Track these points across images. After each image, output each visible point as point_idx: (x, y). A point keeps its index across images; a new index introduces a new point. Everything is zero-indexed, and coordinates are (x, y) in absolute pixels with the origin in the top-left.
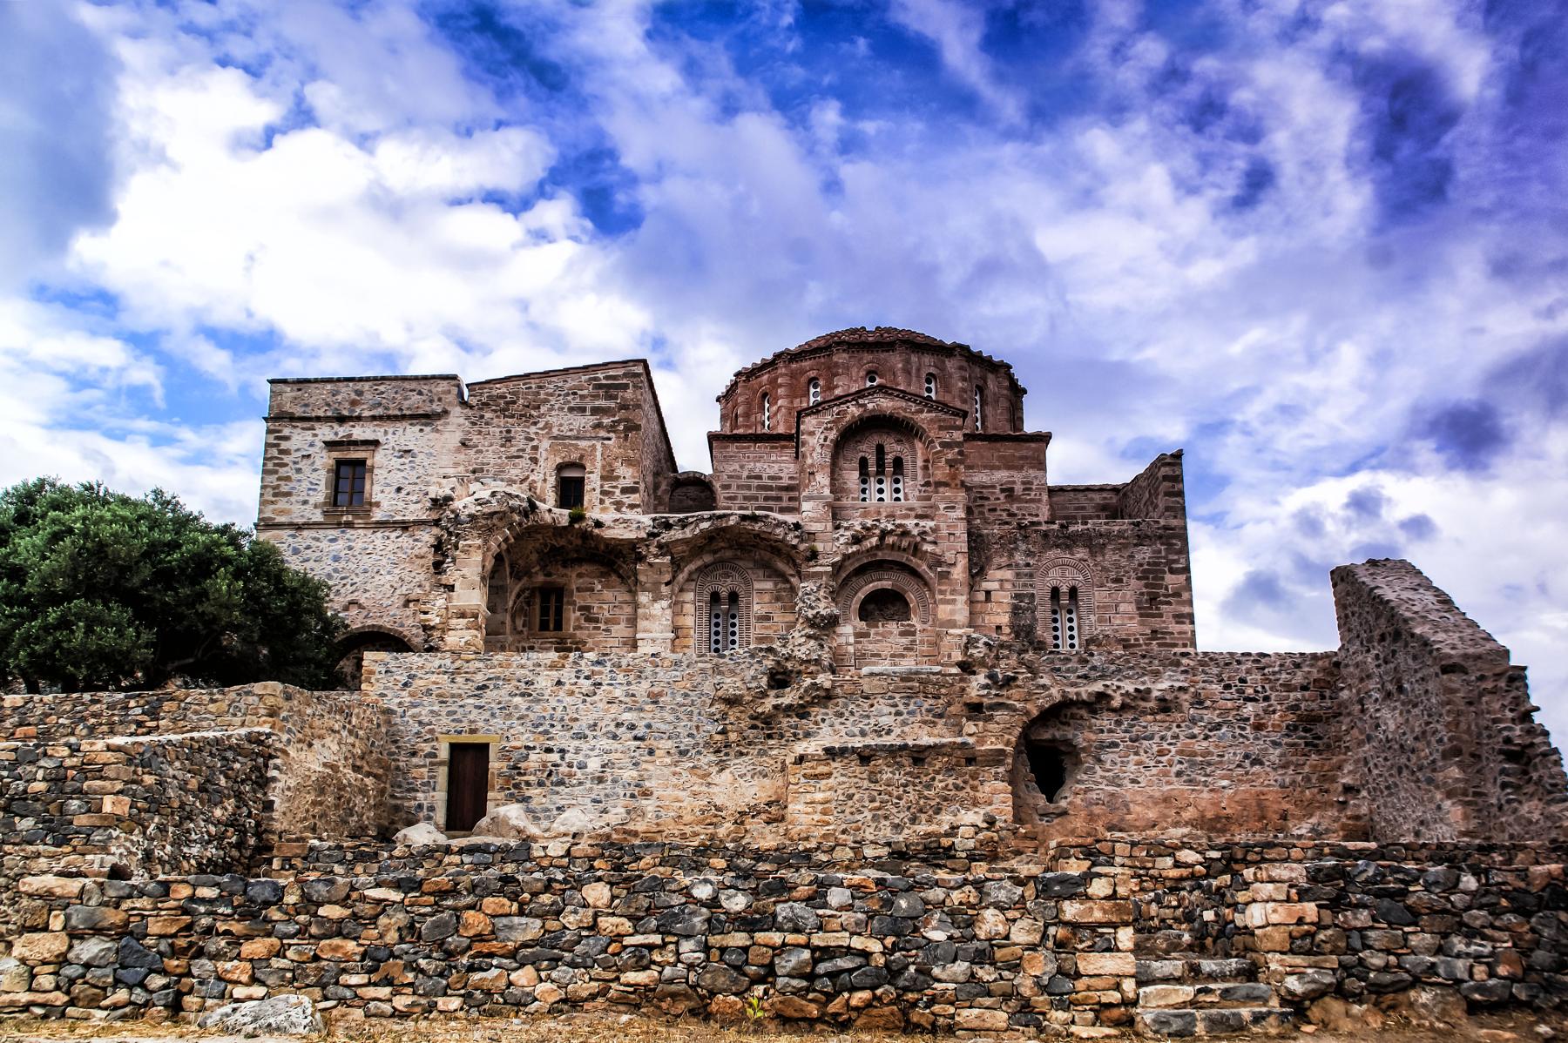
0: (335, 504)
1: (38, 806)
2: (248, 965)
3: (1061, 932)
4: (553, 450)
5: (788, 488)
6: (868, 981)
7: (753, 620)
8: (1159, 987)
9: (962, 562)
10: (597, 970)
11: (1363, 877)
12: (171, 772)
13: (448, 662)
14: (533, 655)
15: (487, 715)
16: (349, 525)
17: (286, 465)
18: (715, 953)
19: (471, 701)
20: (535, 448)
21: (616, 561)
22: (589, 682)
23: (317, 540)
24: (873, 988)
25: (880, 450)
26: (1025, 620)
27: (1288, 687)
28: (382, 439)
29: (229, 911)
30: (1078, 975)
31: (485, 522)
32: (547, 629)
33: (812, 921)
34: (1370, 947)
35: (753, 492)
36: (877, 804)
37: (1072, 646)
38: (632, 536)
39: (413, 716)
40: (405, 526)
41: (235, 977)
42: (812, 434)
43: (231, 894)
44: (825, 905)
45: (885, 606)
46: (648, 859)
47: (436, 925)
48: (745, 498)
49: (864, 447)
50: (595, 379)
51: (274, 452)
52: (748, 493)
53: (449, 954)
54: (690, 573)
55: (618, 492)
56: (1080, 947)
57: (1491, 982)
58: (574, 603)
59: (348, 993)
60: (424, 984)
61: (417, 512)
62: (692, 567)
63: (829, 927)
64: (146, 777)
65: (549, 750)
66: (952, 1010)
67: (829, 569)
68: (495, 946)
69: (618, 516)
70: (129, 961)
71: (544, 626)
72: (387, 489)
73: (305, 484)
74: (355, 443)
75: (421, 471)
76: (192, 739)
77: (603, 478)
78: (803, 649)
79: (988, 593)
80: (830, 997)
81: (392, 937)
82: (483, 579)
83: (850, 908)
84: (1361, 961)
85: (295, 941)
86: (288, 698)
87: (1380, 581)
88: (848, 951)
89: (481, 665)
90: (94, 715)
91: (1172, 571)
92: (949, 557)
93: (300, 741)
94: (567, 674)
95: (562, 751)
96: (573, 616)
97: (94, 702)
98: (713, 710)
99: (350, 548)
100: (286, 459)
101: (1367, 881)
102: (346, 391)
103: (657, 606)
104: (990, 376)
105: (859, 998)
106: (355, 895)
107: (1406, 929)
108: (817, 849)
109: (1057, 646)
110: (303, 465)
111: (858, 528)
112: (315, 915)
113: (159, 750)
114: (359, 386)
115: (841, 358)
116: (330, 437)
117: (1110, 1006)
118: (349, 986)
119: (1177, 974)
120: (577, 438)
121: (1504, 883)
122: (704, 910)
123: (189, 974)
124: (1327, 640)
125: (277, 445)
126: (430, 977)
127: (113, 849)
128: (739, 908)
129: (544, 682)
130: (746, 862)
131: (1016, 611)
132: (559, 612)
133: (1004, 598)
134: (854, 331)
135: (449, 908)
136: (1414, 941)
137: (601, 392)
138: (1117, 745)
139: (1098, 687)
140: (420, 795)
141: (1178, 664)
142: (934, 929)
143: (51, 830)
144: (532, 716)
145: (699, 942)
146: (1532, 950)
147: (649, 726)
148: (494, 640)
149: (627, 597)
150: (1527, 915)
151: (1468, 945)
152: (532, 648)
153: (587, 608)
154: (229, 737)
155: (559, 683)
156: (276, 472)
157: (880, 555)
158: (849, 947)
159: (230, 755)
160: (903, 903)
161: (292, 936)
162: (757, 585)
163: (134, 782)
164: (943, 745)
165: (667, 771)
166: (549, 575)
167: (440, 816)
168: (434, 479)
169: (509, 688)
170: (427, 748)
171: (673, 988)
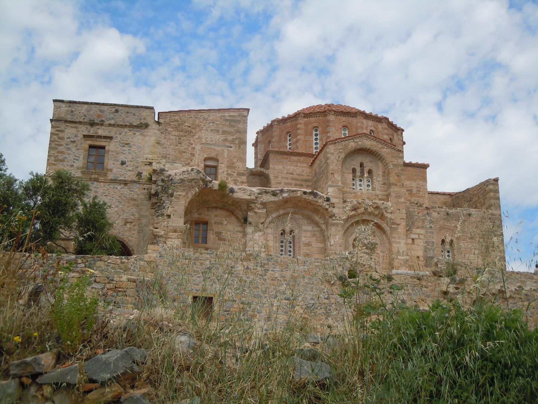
7: (302, 245)
9: (403, 223)
13: (192, 253)
17: (61, 145)
25: (362, 165)
26: (430, 254)
28: (114, 136)
35: (290, 181)
42: (332, 154)
49: (354, 163)
50: (224, 116)
51: (56, 137)
52: (287, 181)
55: (235, 175)
58: (213, 230)
61: (130, 176)
62: (274, 215)
72: (117, 163)
73: (72, 157)
74: (100, 137)
75: (134, 155)
77: (228, 167)
79: (413, 239)
89: (208, 256)
96: (211, 237)
100: (63, 142)
102: (95, 108)
103: (257, 234)
104: (395, 134)
111: (355, 202)
114: (102, 107)
115: (332, 118)
116: (86, 133)
120: (213, 144)
125: (58, 134)
131: (426, 250)
133: (420, 243)
137: (227, 123)
141: (532, 278)
149: (240, 229)
153: (220, 233)
156: (57, 149)
162: (304, 228)
166: (200, 214)
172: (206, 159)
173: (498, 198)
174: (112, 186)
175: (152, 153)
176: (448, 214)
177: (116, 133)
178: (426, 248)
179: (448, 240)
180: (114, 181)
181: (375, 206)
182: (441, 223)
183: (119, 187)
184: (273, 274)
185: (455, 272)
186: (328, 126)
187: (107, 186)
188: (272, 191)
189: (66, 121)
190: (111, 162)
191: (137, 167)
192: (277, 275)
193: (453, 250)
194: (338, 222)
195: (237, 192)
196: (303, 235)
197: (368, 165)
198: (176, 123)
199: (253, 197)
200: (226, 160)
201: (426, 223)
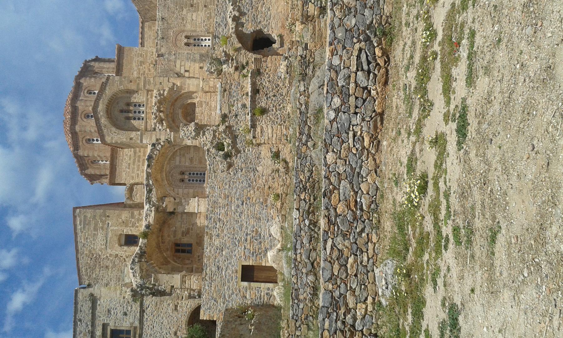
4: (112, 248)
9: (172, 80)
14: (205, 246)
15: (230, 266)
18: (357, 110)
19: (224, 273)
20: (111, 255)
21: (166, 217)
22: (218, 224)
24: (374, 47)
25: (122, 111)
26: (197, 57)
29: (335, 314)
31: (145, 275)
32: (191, 250)
36: (274, 109)
37: (209, 40)
38: (153, 213)
40: (142, 311)
42: (112, 138)
43: (328, 313)
46: (301, 177)
48: (138, 170)
53: (355, 218)
55: (133, 220)
58: (180, 239)
61: (136, 307)
63: (349, 65)
65: (246, 240)
66: (384, 17)
67: (172, 133)
71: (190, 252)
75: (117, 305)
81: (347, 243)
83: (341, 57)
85: (349, 285)
88: (358, 57)
92: (170, 85)
94: (214, 233)
95: (247, 235)
96: (185, 240)
105: (378, 52)
106: (329, 259)
108: (300, 110)
109: (209, 46)
111: (155, 121)
112: (338, 276)
115: (77, 128)
118: (368, 261)
123: (362, 331)
126: (365, 227)
128: (339, 101)
130: (304, 138)
132: (184, 245)
133: (188, 65)
137: (87, 227)
139: (230, 21)
147: (238, 199)
148: (196, 268)
149: (179, 216)
152: (199, 256)
155: (218, 236)
160: (340, 35)
161: (346, 285)
165: (257, 192)
167: (271, 285)
171: (372, 126)
174: (145, 323)
175: (115, 290)
176: (163, 38)
179: (186, 40)
181: (158, 104)
183: (146, 316)
184: (223, 215)
188: (148, 192)
190: (124, 324)
191: (128, 302)
192: (223, 211)
193: (193, 36)
195: (149, 222)
196: (183, 164)
197: (122, 106)
198: (89, 270)
199: (153, 209)
200: (120, 228)
201: (171, 58)
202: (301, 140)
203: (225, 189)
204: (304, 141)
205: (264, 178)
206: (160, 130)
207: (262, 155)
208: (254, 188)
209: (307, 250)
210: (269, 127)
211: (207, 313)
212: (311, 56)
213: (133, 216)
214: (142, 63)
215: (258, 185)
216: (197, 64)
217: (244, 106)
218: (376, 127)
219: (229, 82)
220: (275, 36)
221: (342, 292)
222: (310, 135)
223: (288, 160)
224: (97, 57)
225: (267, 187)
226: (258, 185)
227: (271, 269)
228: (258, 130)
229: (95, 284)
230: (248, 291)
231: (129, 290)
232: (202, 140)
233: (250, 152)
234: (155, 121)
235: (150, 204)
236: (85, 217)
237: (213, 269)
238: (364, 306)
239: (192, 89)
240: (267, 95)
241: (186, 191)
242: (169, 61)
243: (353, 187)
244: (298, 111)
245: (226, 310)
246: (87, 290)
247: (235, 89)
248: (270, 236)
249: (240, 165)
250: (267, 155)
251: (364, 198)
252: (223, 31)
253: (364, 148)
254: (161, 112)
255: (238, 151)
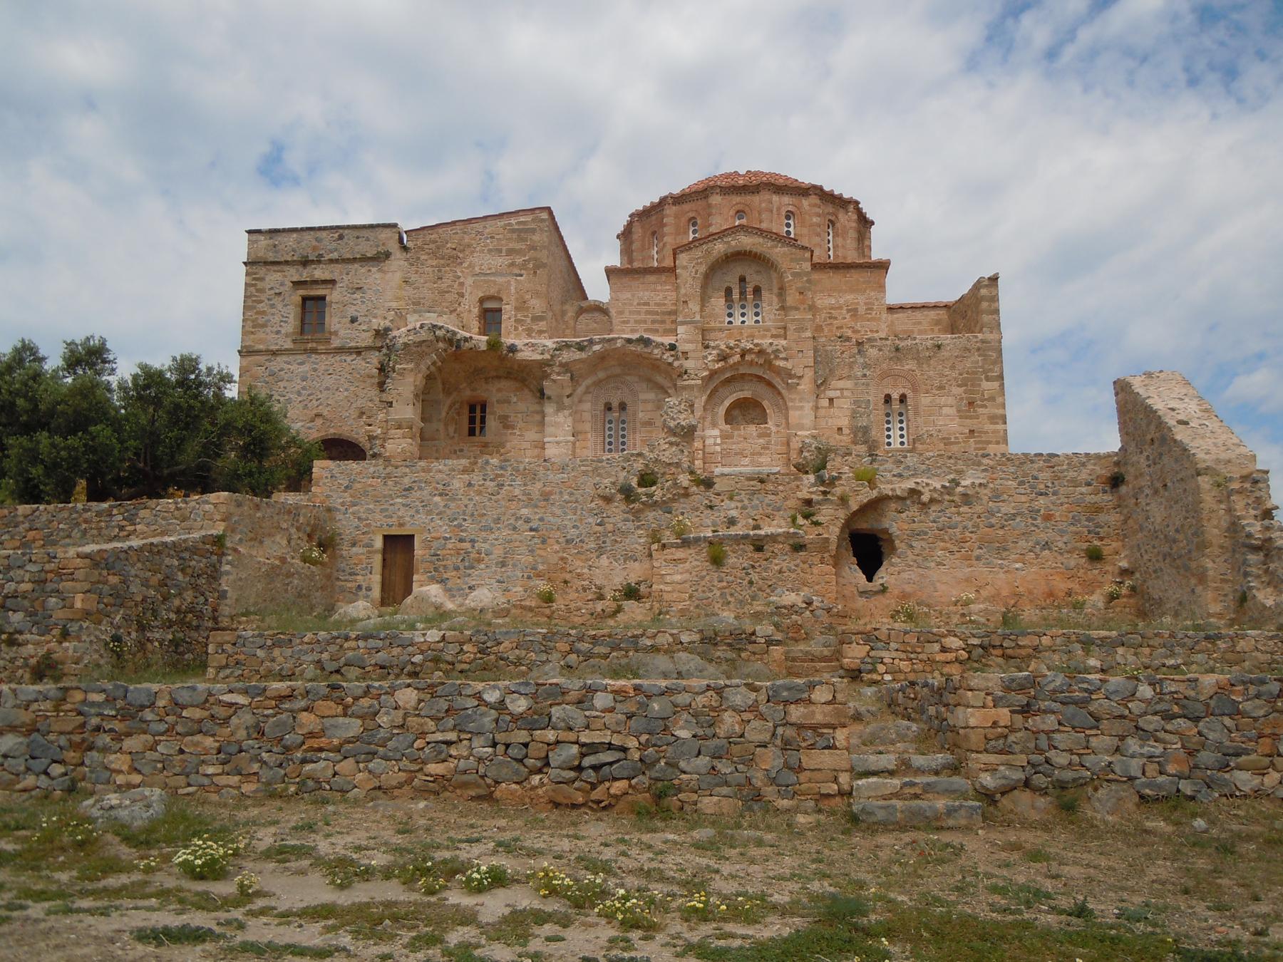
0: (302, 333)
1: (26, 603)
2: (128, 757)
3: (790, 732)
5: (670, 313)
6: (625, 774)
7: (638, 425)
8: (873, 780)
9: (809, 374)
10: (405, 762)
11: (1051, 687)
12: (133, 572)
13: (381, 468)
14: (449, 462)
15: (412, 512)
16: (314, 351)
17: (261, 302)
18: (500, 748)
19: (399, 500)
20: (462, 284)
21: (530, 379)
23: (289, 363)
24: (630, 779)
25: (742, 280)
26: (863, 422)
27: (1075, 483)
29: (113, 713)
30: (800, 769)
31: (414, 350)
33: (581, 721)
34: (1055, 748)
35: (643, 317)
36: (725, 584)
38: (539, 357)
39: (353, 513)
40: (358, 351)
41: (117, 767)
42: (685, 268)
44: (592, 708)
45: (746, 411)
47: (277, 725)
48: (636, 322)
50: (509, 224)
51: (252, 289)
52: (639, 317)
53: (287, 749)
54: (588, 387)
55: (529, 320)
56: (803, 744)
57: (1161, 779)
58: (494, 413)
59: (206, 781)
60: (266, 775)
61: (366, 339)
62: (589, 381)
64: (110, 578)
65: (461, 541)
66: (695, 797)
68: (323, 742)
69: (528, 342)
70: (37, 753)
71: (472, 432)
73: (277, 318)
74: (315, 282)
76: (152, 544)
77: (517, 309)
78: (667, 453)
79: (831, 400)
80: (594, 786)
81: (242, 734)
82: (416, 396)
83: (612, 710)
84: (1047, 761)
86: (239, 505)
87: (1152, 391)
88: (610, 747)
90: (86, 521)
91: (988, 379)
93: (251, 540)
94: (476, 478)
95: (473, 541)
96: (491, 423)
97: (85, 510)
98: (593, 505)
99: (315, 370)
101: (1054, 691)
102: (308, 237)
105: (618, 787)
106: (212, 700)
107: (1088, 732)
109: (889, 444)
110: (276, 301)
111: (723, 347)
113: (123, 556)
114: (319, 234)
115: (716, 199)
117: (828, 796)
118: (207, 775)
119: (891, 767)
121: (1176, 692)
122: (493, 711)
123: (82, 764)
124: (1111, 441)
126: (271, 768)
127: (84, 638)
128: (521, 710)
129: (457, 484)
130: (584, 646)
131: (854, 415)
133: (845, 404)
134: (727, 176)
135: (287, 710)
136: (1094, 742)
137: (515, 236)
138: (926, 534)
139: (910, 484)
140: (359, 577)
141: (979, 464)
142: (682, 728)
143: (35, 623)
144: (448, 512)
145: (487, 739)
146: (1198, 751)
147: (541, 519)
148: (427, 444)
149: (537, 407)
150: (1196, 720)
151: (1142, 746)
152: (461, 450)
154: (185, 541)
155: (470, 485)
157: (742, 371)
158: (610, 744)
159: (186, 555)
160: (656, 706)
161: (162, 734)
162: (642, 396)
163: (99, 582)
164: (779, 535)
167: (376, 593)
168: (379, 312)
169: (429, 489)
170: (365, 539)
171: (465, 778)
172: (482, 301)
173: (997, 311)
174: (338, 358)
175: (398, 299)
176: (897, 349)
177: (341, 273)
178: (854, 412)
179: (895, 396)
180: (341, 350)
181: (757, 349)
182: (885, 366)
183: (349, 359)
185: (823, 466)
186: (710, 215)
187: (331, 359)
189: (266, 263)
192: (517, 492)
194: (693, 382)
197: (753, 279)
198: (432, 246)
199: (547, 356)
201: (856, 369)
202: (581, 639)
203: (561, 493)
204: (580, 646)
205: (586, 571)
206: (706, 357)
207: (630, 564)
208: (564, 550)
209: (363, 660)
210: (686, 576)
211: (325, 474)
212: (754, 653)
213: (536, 319)
214: (854, 312)
215: (570, 558)
216: (846, 422)
217: (732, 522)
218: (465, 785)
219: (781, 488)
220: (882, 576)
221: (152, 725)
222: (590, 657)
223: (620, 617)
224: (873, 223)
225: (568, 577)
226: (570, 558)
227: (408, 591)
228: (680, 554)
229: (407, 260)
230: (365, 550)
231: (388, 323)
232: (662, 442)
233: (637, 541)
234: (723, 347)
235: (556, 349)
236: (533, 231)
237: (406, 480)
238: (125, 768)
239: (794, 415)
240: (753, 567)
241: (587, 416)
242: (851, 366)
243: (349, 742)
244: (639, 632)
245: (329, 510)
246: (397, 245)
247: (767, 501)
248: (470, 588)
249: (611, 520)
250: (632, 575)
251: (327, 766)
252: (885, 470)
253: (424, 763)
254: (743, 356)
255: (637, 515)
